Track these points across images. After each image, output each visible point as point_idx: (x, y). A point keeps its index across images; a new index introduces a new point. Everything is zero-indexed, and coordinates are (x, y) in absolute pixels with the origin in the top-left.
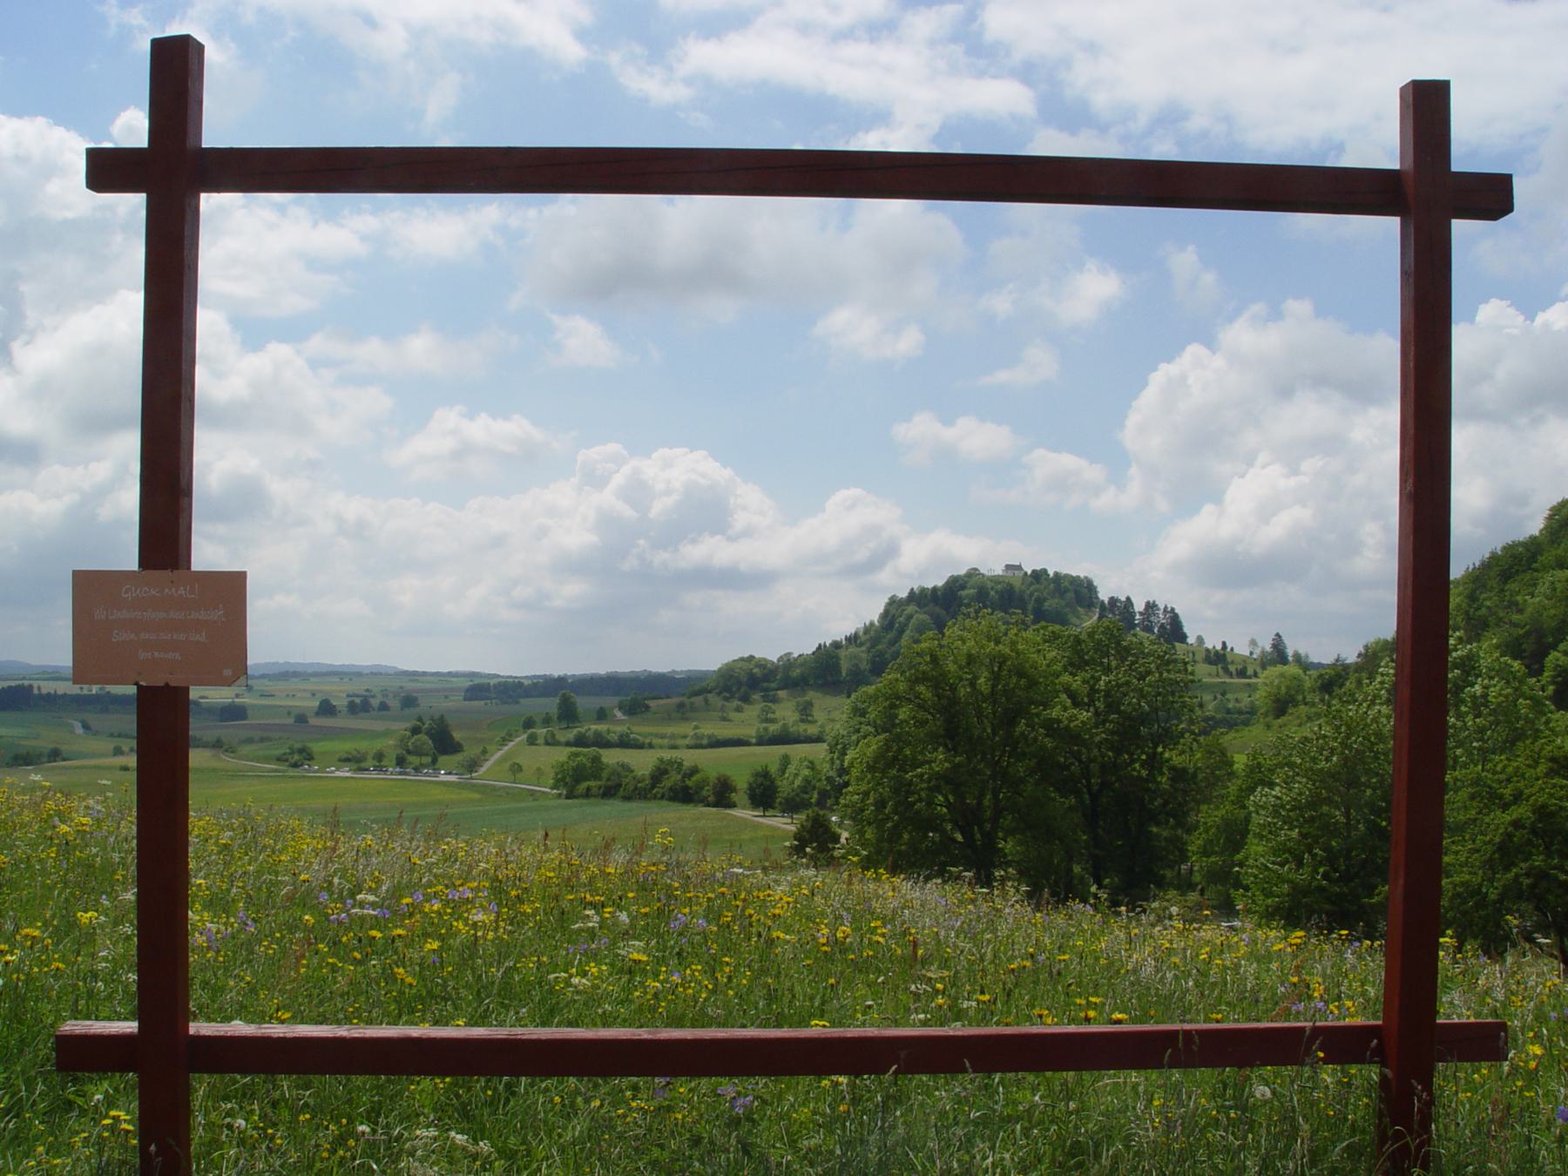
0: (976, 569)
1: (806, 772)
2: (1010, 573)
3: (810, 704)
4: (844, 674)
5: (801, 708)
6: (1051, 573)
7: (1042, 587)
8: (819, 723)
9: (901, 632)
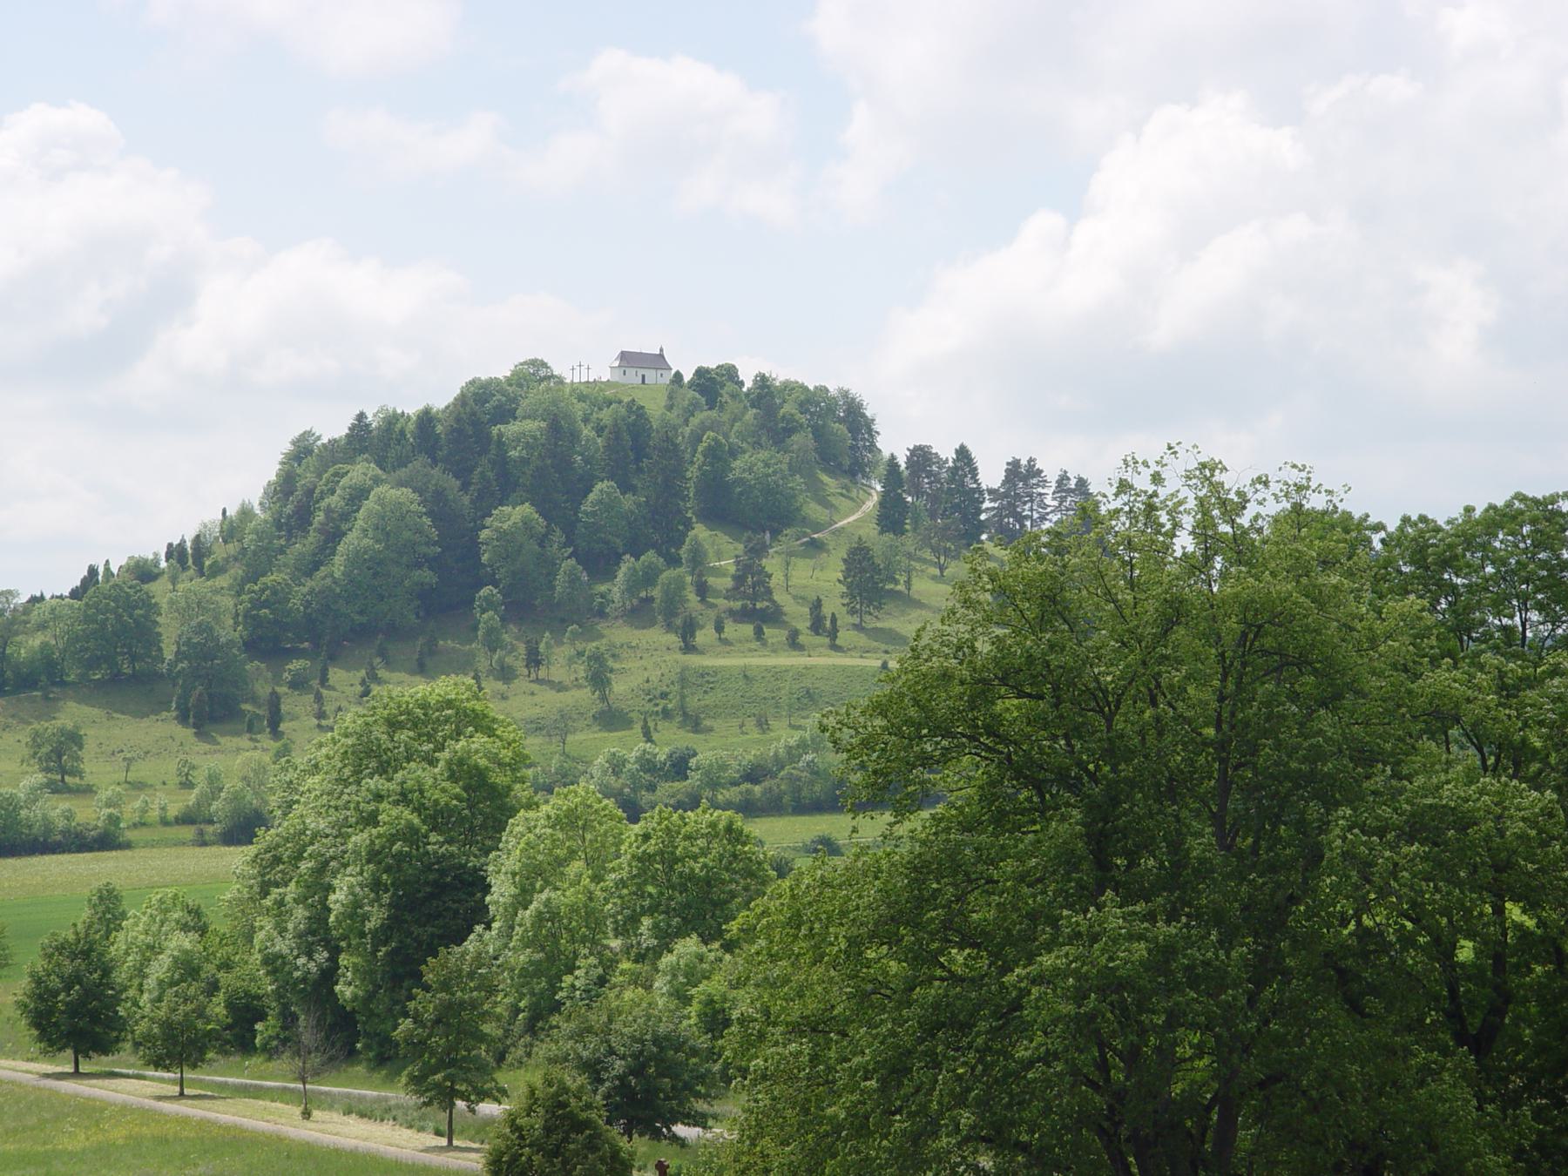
0: (539, 364)
1: (184, 942)
2: (633, 377)
3: (74, 739)
4: (169, 653)
5: (46, 749)
6: (748, 380)
7: (725, 417)
8: (104, 795)
9: (333, 536)
